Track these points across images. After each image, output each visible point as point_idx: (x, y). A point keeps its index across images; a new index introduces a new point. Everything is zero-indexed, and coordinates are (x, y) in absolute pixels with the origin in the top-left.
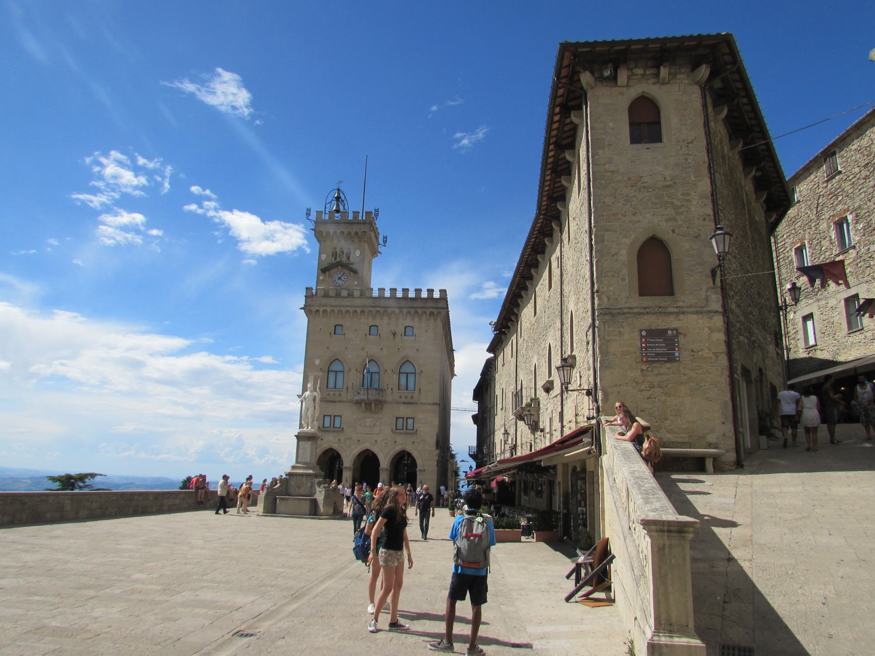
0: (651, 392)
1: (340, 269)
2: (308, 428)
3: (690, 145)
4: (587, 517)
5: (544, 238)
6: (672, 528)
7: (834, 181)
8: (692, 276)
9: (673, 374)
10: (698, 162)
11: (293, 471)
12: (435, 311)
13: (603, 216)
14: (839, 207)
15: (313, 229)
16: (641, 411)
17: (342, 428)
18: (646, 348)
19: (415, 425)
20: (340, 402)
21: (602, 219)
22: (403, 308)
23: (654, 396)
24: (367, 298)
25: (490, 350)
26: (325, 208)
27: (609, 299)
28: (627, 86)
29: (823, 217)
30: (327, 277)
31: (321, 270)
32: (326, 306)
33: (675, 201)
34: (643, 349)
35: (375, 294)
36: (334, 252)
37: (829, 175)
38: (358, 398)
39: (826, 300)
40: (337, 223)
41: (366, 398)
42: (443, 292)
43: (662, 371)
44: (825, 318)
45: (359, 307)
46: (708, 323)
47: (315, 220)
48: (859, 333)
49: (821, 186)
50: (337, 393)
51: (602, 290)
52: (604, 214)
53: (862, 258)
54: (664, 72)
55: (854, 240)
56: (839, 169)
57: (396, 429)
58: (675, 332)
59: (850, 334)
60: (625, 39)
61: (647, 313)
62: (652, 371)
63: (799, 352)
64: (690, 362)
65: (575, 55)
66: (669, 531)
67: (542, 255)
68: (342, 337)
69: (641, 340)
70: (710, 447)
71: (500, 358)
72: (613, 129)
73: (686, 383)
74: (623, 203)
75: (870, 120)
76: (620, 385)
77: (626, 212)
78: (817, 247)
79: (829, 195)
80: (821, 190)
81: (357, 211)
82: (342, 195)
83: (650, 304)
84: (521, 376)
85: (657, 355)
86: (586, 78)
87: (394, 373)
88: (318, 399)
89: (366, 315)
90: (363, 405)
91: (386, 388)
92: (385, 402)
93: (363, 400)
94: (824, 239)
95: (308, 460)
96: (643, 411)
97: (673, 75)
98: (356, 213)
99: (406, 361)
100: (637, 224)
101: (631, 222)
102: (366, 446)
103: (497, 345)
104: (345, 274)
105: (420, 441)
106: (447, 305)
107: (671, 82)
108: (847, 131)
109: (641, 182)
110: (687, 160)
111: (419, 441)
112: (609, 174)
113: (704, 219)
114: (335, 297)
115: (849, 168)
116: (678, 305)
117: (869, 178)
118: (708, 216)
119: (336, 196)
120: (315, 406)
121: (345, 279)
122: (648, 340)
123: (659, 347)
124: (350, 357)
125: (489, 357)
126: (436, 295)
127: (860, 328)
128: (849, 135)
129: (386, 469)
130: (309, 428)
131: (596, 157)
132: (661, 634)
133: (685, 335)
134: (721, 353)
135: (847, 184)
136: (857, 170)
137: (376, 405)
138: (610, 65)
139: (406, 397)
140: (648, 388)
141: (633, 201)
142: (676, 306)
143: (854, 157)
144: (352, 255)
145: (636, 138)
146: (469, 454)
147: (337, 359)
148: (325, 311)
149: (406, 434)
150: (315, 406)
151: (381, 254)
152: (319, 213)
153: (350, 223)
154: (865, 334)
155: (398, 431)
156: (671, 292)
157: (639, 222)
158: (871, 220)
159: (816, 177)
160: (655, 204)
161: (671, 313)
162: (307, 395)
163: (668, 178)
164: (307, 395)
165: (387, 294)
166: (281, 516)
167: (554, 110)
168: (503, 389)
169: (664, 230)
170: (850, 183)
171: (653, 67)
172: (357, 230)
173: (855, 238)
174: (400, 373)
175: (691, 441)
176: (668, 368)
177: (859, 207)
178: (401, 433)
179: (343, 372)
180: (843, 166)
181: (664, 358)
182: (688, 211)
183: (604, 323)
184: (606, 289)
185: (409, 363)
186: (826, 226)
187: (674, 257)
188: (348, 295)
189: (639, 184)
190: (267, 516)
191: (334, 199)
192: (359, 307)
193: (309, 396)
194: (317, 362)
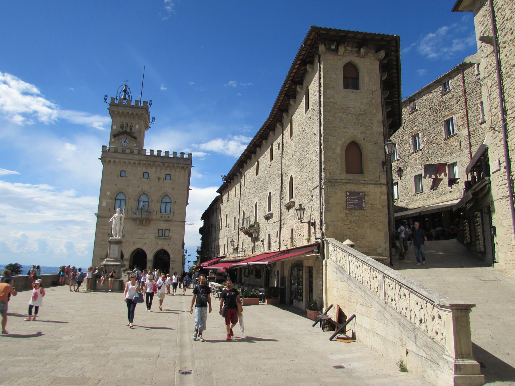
0: (350, 225)
2: (116, 236)
3: (374, 93)
4: (303, 291)
6: (462, 308)
7: (413, 114)
8: (372, 164)
9: (362, 216)
11: (107, 263)
12: (185, 166)
13: (328, 127)
14: (415, 128)
15: (108, 109)
16: (345, 235)
18: (349, 201)
19: (170, 234)
21: (328, 129)
24: (142, 155)
25: (218, 191)
26: (117, 96)
27: (330, 173)
28: (343, 56)
29: (406, 132)
32: (116, 158)
33: (365, 123)
35: (148, 153)
36: (121, 125)
37: (411, 111)
38: (135, 216)
39: (405, 176)
40: (125, 106)
41: (139, 216)
43: (356, 214)
44: (404, 185)
47: (110, 103)
48: (421, 194)
49: (406, 116)
51: (326, 168)
52: (329, 126)
53: (425, 156)
54: (363, 51)
55: (422, 146)
56: (417, 109)
57: (158, 236)
59: (416, 194)
60: (355, 31)
61: (350, 183)
62: (351, 214)
63: (400, 204)
64: (370, 210)
65: (318, 34)
66: (461, 309)
67: (266, 141)
68: (126, 178)
69: (346, 197)
70: (378, 255)
71: (225, 197)
72: (335, 79)
75: (433, 86)
76: (335, 221)
77: (340, 126)
78: (402, 148)
79: (410, 121)
80: (406, 118)
81: (146, 101)
84: (243, 208)
85: (354, 205)
86: (322, 48)
87: (158, 202)
88: (123, 219)
90: (138, 221)
92: (152, 220)
93: (138, 218)
94: (406, 144)
95: (116, 256)
96: (346, 235)
97: (366, 53)
98: (137, 102)
99: (166, 195)
100: (346, 134)
101: (342, 132)
103: (224, 189)
107: (365, 57)
108: (422, 89)
110: (372, 101)
111: (172, 243)
112: (332, 104)
113: (380, 134)
114: (121, 153)
115: (422, 109)
117: (431, 115)
118: (382, 132)
119: (124, 89)
121: (128, 142)
123: (355, 201)
124: (130, 191)
125: (218, 195)
127: (421, 191)
128: (422, 92)
130: (117, 236)
131: (325, 94)
132: (459, 360)
134: (386, 206)
135: (420, 117)
136: (425, 110)
137: (146, 221)
138: (335, 42)
139: (165, 217)
143: (424, 104)
145: (346, 86)
147: (121, 192)
148: (115, 162)
149: (164, 239)
151: (151, 128)
152: (113, 99)
153: (133, 107)
154: (424, 195)
155: (159, 237)
156: (361, 172)
157: (347, 132)
158: (430, 137)
159: (404, 111)
160: (355, 123)
161: (362, 184)
162: (116, 216)
163: (362, 110)
164: (116, 216)
167: (297, 62)
168: (227, 215)
169: (359, 137)
170: (421, 116)
171: (356, 47)
172: (138, 112)
173: (422, 145)
175: (369, 252)
176: (359, 213)
177: (425, 130)
178: (161, 239)
179: (125, 200)
180: (418, 107)
183: (327, 187)
184: (329, 168)
185: (169, 198)
186: (407, 137)
187: (364, 153)
188: (130, 152)
189: (348, 111)
191: (123, 91)
193: (117, 216)
194: (109, 193)
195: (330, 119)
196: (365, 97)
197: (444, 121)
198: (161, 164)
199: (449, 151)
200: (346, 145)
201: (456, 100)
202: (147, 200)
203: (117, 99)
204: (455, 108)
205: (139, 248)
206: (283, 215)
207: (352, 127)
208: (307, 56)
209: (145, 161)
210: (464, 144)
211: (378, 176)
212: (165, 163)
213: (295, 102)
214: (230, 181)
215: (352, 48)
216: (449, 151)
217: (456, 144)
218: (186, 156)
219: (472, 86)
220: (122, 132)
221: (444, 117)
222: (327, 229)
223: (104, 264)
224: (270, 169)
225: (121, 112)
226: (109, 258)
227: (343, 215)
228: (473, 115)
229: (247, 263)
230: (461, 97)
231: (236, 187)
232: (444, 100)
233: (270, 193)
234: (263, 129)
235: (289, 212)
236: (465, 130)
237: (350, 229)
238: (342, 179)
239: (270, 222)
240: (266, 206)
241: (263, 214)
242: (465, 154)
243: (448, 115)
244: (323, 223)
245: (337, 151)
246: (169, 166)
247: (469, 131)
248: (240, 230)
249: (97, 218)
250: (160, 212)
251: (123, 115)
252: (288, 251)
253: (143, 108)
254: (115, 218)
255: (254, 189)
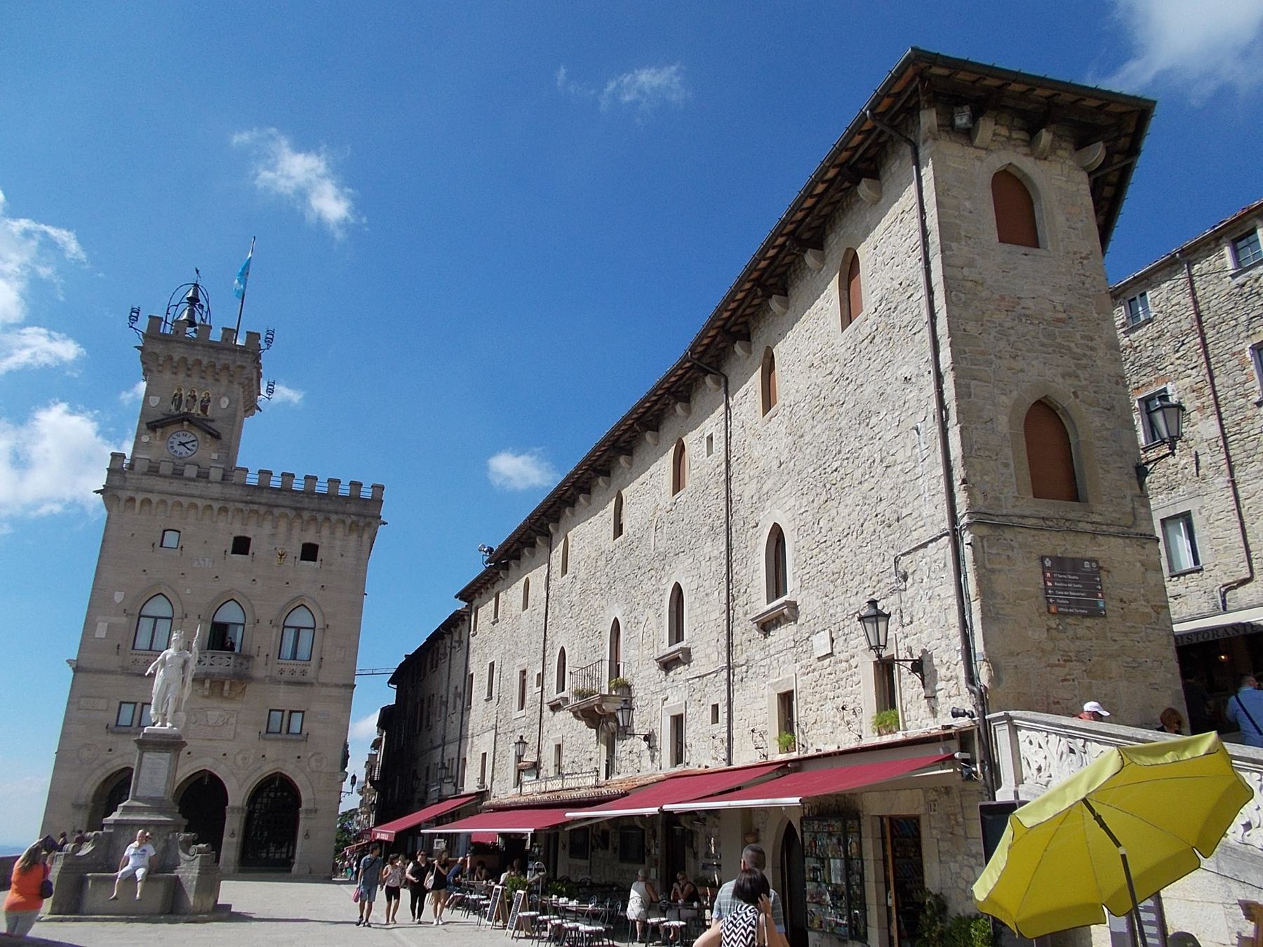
0: (1067, 669)
1: (185, 427)
2: (164, 725)
3: (1085, 262)
5: (676, 403)
8: (1109, 472)
10: (1099, 291)
15: (139, 348)
18: (1054, 588)
21: (965, 358)
23: (1073, 677)
26: (168, 313)
30: (158, 439)
31: (148, 424)
32: (151, 492)
34: (1050, 592)
36: (176, 395)
40: (191, 343)
43: (1081, 632)
45: (217, 499)
46: (1140, 555)
47: (145, 332)
52: (967, 349)
54: (1046, 137)
57: (267, 732)
58: (1094, 565)
62: (1065, 631)
69: (1044, 574)
71: (485, 612)
73: (1119, 656)
74: (995, 337)
76: (1018, 655)
77: (1000, 351)
82: (200, 296)
83: (1052, 512)
84: (559, 640)
90: (207, 685)
91: (254, 653)
96: (1058, 703)
100: (1020, 375)
104: (195, 443)
109: (1020, 307)
110: (1083, 284)
112: (969, 285)
116: (1094, 520)
119: (190, 294)
122: (1055, 575)
129: (238, 809)
130: (169, 725)
131: (948, 253)
133: (1109, 572)
140: (1062, 662)
141: (1010, 335)
142: (1089, 520)
152: (155, 321)
157: (1022, 371)
166: (96, 920)
168: (492, 665)
169: (1062, 390)
176: (1088, 628)
178: (277, 740)
179: (171, 618)
181: (1082, 609)
182: (1092, 365)
183: (982, 538)
184: (979, 478)
185: (307, 611)
190: (62, 920)
194: (119, 597)
195: (968, 328)
196: (1063, 270)
197: (1139, 400)
198: (292, 514)
199: (1163, 480)
200: (1023, 411)
201: (1172, 343)
202: (242, 621)
203: (166, 322)
204: (1172, 364)
205: (205, 770)
206: (737, 652)
207: (1035, 354)
208: (865, 151)
209: (242, 502)
210: (1210, 461)
211: (1129, 509)
212: (304, 509)
213: (786, 306)
214: (507, 564)
215: (1010, 130)
216: (1163, 480)
217: (1183, 462)
218: (366, 493)
219: (1221, 305)
220: (173, 416)
221: (1138, 388)
222: (995, 678)
223: (115, 820)
224: (673, 516)
225: (176, 358)
226: (135, 799)
227: (1038, 635)
228: (1231, 382)
229: (655, 810)
230: (1187, 335)
231: (527, 582)
232: (1136, 344)
233: (678, 591)
234: (655, 395)
235: (769, 640)
236: (1210, 423)
237: (1065, 680)
238: (1023, 517)
239: (683, 677)
240: (660, 625)
241: (646, 652)
242: (1214, 488)
243: (1150, 383)
244: (979, 658)
245: (999, 428)
246: (314, 519)
247: (1222, 426)
248: (546, 707)
249: (72, 674)
250: (279, 658)
251: (184, 366)
252: (797, 764)
253: (248, 352)
254: (164, 663)
255: (604, 579)
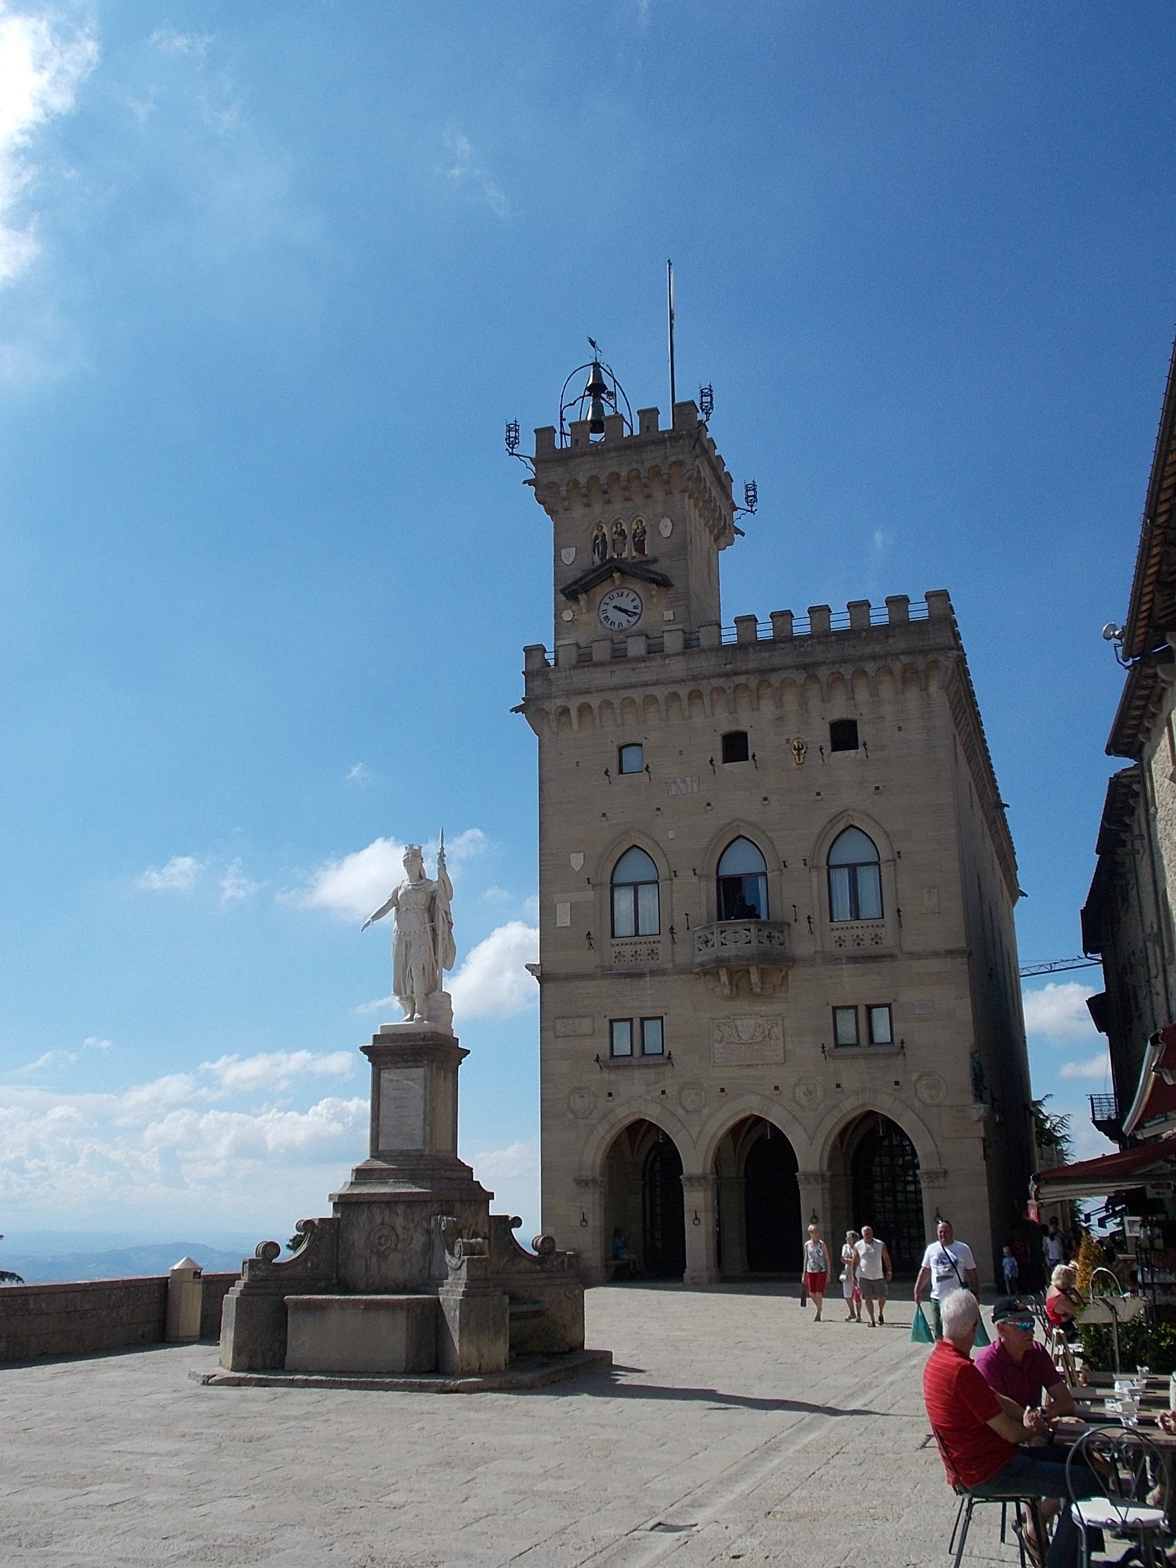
1: (617, 582)
15: (530, 482)
17: (666, 1054)
20: (653, 973)
22: (816, 665)
25: (1114, 748)
30: (584, 611)
35: (729, 636)
42: (939, 598)
45: (682, 681)
47: (533, 455)
50: (643, 947)
89: (706, 700)
91: (789, 917)
93: (720, 962)
98: (649, 415)
102: (751, 1105)
105: (920, 1078)
106: (957, 636)
111: (914, 1076)
114: (609, 664)
120: (434, 930)
124: (671, 835)
126: (919, 611)
129: (815, 1175)
137: (763, 974)
139: (858, 941)
144: (647, 537)
146: (1094, 1122)
150: (434, 930)
151: (743, 534)
152: (544, 435)
153: (634, 445)
165: (765, 631)
174: (830, 867)
192: (682, 681)
194: (577, 861)
